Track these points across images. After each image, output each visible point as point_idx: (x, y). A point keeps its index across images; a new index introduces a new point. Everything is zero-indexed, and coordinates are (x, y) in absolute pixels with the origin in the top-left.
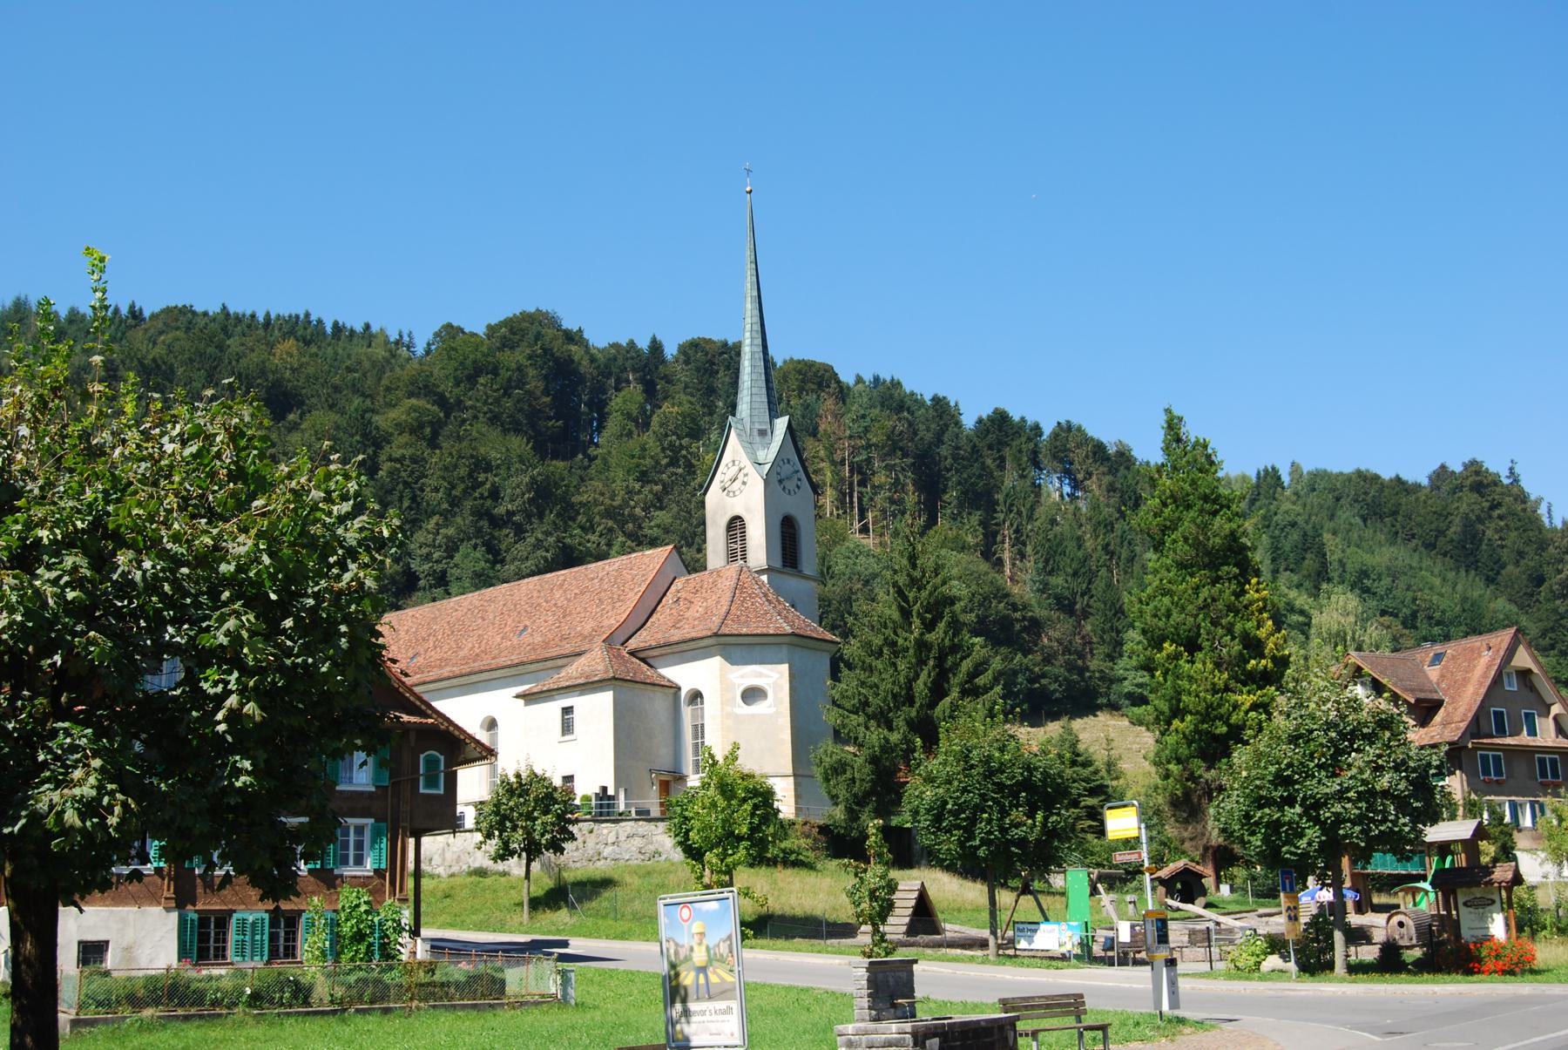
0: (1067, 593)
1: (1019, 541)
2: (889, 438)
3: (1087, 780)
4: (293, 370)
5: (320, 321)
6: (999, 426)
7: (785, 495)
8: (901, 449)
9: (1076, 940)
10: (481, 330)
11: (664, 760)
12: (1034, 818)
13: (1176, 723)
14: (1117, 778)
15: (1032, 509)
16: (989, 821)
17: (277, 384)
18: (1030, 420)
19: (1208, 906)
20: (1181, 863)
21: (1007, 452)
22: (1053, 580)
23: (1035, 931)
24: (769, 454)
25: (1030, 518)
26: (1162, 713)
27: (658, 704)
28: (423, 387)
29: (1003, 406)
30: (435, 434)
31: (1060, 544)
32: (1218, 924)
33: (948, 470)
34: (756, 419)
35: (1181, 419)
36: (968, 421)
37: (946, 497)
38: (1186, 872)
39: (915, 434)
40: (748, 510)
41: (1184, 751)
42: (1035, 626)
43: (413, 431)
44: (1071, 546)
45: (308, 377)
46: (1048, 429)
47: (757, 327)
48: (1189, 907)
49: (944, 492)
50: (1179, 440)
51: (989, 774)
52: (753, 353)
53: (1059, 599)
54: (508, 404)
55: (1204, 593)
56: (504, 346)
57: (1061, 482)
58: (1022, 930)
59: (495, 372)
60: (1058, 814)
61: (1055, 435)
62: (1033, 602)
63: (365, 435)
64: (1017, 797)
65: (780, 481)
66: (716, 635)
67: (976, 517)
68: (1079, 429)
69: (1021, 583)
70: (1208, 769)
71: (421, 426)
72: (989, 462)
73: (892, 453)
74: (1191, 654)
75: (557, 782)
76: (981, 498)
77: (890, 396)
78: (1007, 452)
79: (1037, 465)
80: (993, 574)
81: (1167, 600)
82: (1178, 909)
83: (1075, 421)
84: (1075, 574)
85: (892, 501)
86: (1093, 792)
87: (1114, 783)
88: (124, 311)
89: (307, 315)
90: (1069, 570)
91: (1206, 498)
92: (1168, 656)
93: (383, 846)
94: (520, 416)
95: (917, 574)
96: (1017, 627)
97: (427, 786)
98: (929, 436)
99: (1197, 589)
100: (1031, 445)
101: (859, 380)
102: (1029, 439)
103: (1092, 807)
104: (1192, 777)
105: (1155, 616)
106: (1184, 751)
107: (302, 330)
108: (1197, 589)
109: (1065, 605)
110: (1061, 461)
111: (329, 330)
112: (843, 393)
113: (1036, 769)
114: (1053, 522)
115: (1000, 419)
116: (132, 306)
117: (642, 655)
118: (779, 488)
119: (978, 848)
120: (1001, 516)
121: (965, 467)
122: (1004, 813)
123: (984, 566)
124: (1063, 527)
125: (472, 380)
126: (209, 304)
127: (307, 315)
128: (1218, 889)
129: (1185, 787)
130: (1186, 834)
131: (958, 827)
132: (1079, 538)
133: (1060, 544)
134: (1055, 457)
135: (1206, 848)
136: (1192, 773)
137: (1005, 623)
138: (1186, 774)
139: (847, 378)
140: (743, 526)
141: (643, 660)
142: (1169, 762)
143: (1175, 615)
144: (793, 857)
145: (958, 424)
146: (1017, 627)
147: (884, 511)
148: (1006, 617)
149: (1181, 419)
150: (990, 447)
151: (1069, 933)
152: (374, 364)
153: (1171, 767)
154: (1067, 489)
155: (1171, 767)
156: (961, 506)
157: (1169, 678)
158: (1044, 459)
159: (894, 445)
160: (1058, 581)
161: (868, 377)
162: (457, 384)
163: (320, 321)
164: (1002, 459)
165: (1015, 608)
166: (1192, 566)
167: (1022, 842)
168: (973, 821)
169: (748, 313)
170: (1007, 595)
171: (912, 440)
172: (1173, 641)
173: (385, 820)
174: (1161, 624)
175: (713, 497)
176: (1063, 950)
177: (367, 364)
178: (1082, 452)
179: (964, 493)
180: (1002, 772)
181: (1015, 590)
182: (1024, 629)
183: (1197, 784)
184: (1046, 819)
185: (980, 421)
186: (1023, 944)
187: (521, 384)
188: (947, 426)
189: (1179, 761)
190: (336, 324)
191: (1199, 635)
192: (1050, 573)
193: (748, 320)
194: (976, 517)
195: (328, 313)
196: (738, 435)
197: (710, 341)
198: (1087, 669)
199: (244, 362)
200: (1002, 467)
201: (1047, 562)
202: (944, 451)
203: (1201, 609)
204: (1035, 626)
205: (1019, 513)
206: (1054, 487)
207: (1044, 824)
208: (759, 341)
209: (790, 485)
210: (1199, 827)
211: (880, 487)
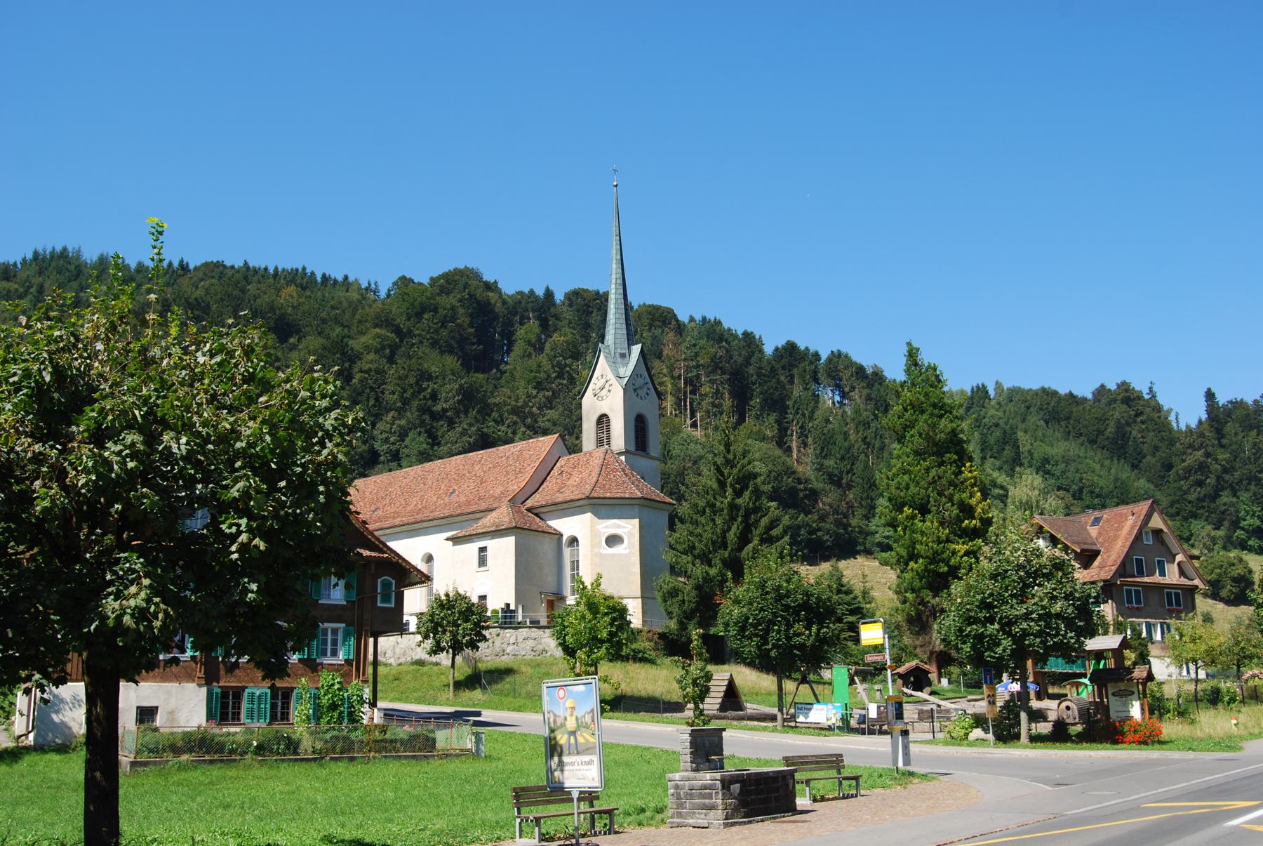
1: (803, 435)
3: (848, 604)
4: (294, 308)
5: (313, 273)
6: (790, 352)
7: (638, 400)
9: (839, 716)
11: (550, 586)
13: (912, 564)
15: (813, 412)
16: (779, 632)
18: (812, 349)
19: (932, 693)
20: (914, 663)
21: (795, 371)
22: (827, 462)
24: (627, 371)
25: (811, 418)
27: (547, 545)
28: (384, 320)
29: (792, 339)
33: (754, 384)
36: (769, 349)
37: (752, 403)
39: (731, 358)
40: (612, 410)
41: (917, 584)
42: (814, 495)
44: (839, 438)
45: (304, 312)
46: (824, 356)
47: (620, 281)
49: (751, 399)
50: (916, 365)
51: (779, 598)
53: (830, 475)
55: (933, 472)
59: (435, 310)
61: (830, 360)
66: (588, 498)
67: (772, 418)
68: (846, 356)
70: (934, 597)
71: (383, 348)
72: (782, 378)
73: (714, 372)
74: (923, 515)
76: (776, 404)
77: (713, 331)
78: (795, 371)
79: (817, 381)
80: (784, 458)
81: (906, 477)
83: (844, 350)
84: (842, 458)
88: (176, 264)
89: (304, 269)
91: (935, 406)
94: (452, 342)
95: (731, 457)
96: (801, 495)
98: (740, 360)
99: (927, 470)
100: (813, 367)
101: (692, 319)
102: (811, 363)
103: (852, 623)
104: (923, 603)
106: (917, 584)
108: (927, 470)
109: (834, 480)
111: (319, 279)
112: (680, 328)
114: (827, 421)
115: (791, 348)
116: (182, 261)
118: (634, 395)
122: (789, 626)
123: (778, 452)
124: (835, 424)
126: (234, 259)
127: (304, 269)
128: (939, 681)
129: (917, 609)
132: (845, 433)
134: (829, 375)
135: (932, 653)
136: (922, 600)
137: (793, 492)
139: (683, 317)
140: (608, 421)
141: (536, 515)
145: (761, 351)
146: (801, 495)
150: (784, 368)
152: (350, 303)
153: (907, 595)
154: (837, 398)
155: (907, 595)
156: (762, 409)
158: (822, 376)
159: (715, 366)
160: (830, 463)
164: (792, 377)
167: (802, 647)
168: (767, 631)
170: (794, 473)
172: (910, 506)
174: (902, 494)
175: (587, 400)
176: (830, 723)
179: (765, 400)
182: (806, 497)
184: (819, 630)
185: (777, 349)
188: (753, 353)
189: (913, 591)
190: (324, 276)
192: (825, 458)
194: (772, 418)
195: (318, 267)
197: (587, 290)
198: (850, 525)
199: (259, 301)
200: (791, 382)
201: (822, 449)
202: (751, 370)
204: (814, 495)
205: (804, 415)
206: (829, 397)
211: (706, 395)
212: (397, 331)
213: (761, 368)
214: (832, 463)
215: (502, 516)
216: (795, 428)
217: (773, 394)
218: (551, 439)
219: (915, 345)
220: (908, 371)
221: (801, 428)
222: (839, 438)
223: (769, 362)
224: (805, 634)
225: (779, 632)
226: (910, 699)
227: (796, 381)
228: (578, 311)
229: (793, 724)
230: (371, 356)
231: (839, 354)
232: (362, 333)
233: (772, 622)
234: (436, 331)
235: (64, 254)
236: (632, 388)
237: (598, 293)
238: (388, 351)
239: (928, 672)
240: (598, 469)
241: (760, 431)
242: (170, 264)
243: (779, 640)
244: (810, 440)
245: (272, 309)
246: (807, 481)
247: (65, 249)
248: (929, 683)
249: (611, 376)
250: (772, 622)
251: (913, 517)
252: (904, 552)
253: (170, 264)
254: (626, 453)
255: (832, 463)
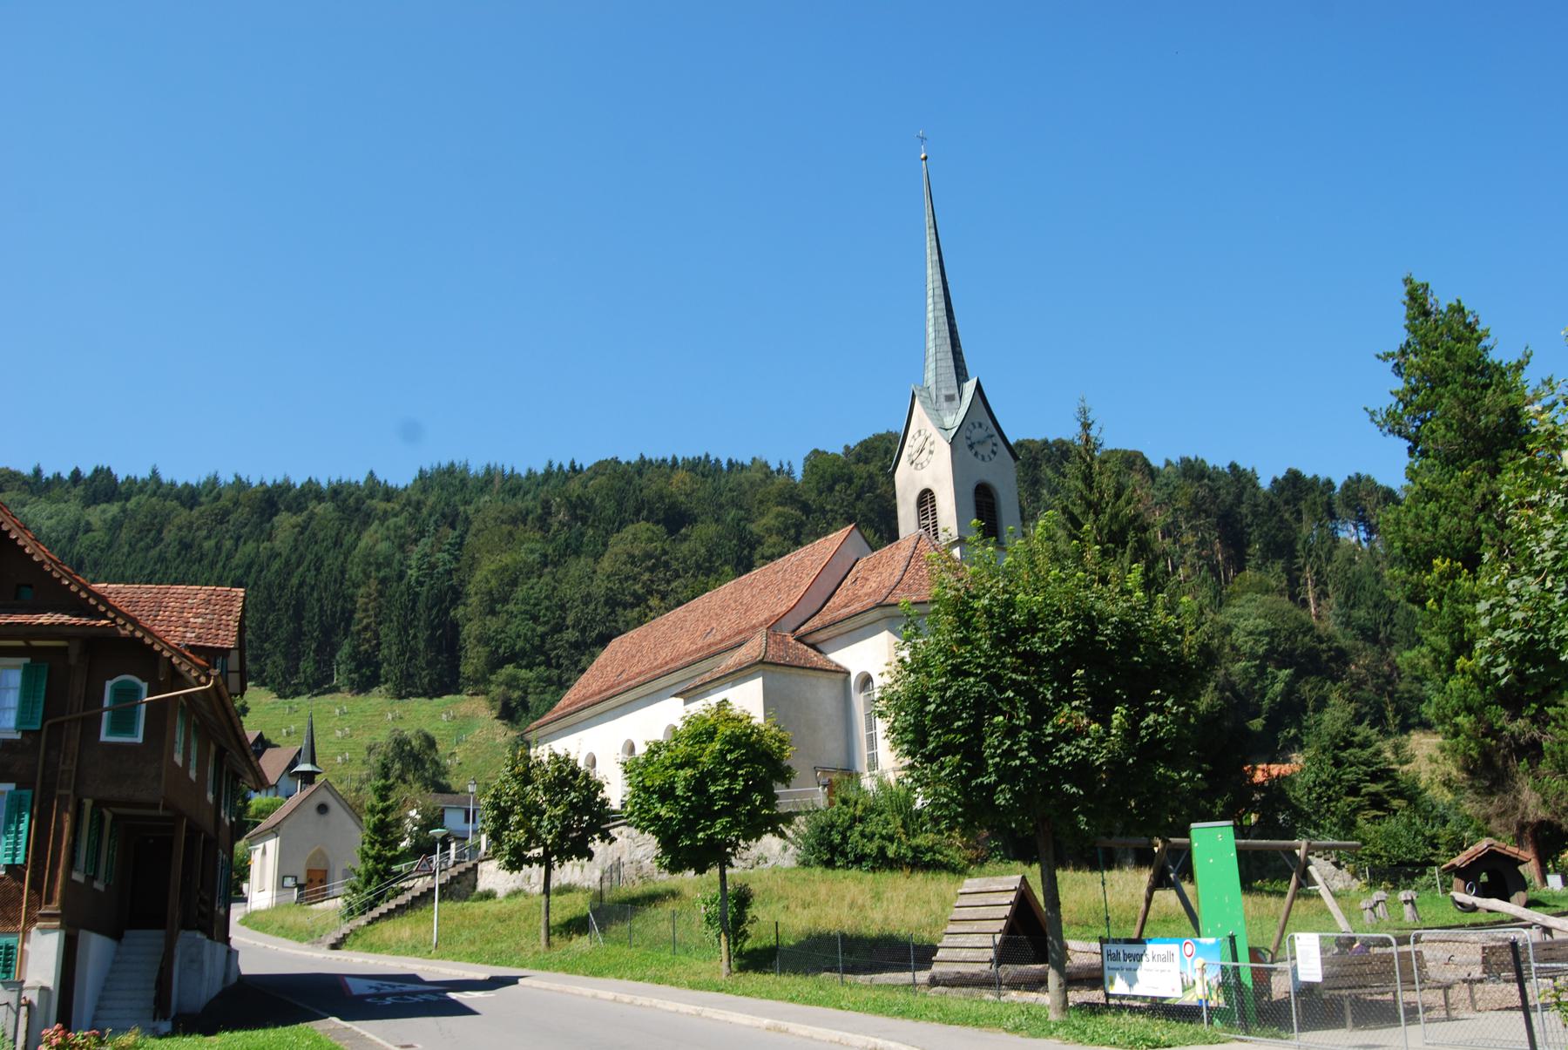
0: (1369, 624)
1: (1320, 581)
2: (1192, 502)
3: (1367, 763)
4: (687, 495)
5: (717, 460)
6: (1294, 483)
7: (978, 461)
8: (1205, 511)
9: (1214, 976)
10: (840, 451)
11: (835, 758)
12: (1106, 722)
13: (1461, 662)
14: (1407, 762)
15: (1330, 552)
16: (1011, 732)
17: (673, 506)
18: (1322, 476)
19: (1530, 904)
20: (1484, 844)
21: (1302, 505)
22: (1356, 613)
23: (1138, 958)
24: (954, 420)
25: (1329, 560)
26: (1441, 652)
27: (823, 692)
28: (790, 496)
29: (1295, 467)
30: (798, 534)
31: (1359, 580)
32: (1547, 930)
33: (1249, 526)
34: (942, 385)
35: (1426, 287)
36: (1265, 483)
37: (1250, 551)
38: (1491, 856)
39: (1217, 497)
40: (936, 480)
41: (1475, 696)
42: (1342, 656)
43: (779, 533)
44: (1369, 580)
45: (699, 500)
46: (1339, 483)
47: (940, 291)
48: (1494, 903)
49: (1248, 545)
50: (1427, 314)
51: (1008, 637)
52: (936, 318)
53: (1363, 630)
54: (860, 505)
55: (1481, 488)
56: (859, 461)
57: (1356, 527)
58: (1115, 957)
59: (850, 481)
60: (1160, 710)
61: (1346, 486)
62: (1339, 634)
63: (741, 539)
64: (1067, 680)
65: (971, 446)
66: (879, 606)
67: (1279, 566)
68: (1368, 479)
69: (1326, 617)
70: (1513, 718)
71: (787, 529)
72: (1287, 516)
73: (1197, 515)
74: (1472, 570)
75: (581, 764)
76: (1282, 549)
77: (1193, 470)
78: (1302, 505)
79: (1333, 516)
80: (1297, 611)
81: (1432, 506)
82: (1474, 909)
83: (1364, 473)
84: (1376, 606)
85: (1199, 557)
86: (1375, 777)
87: (1406, 768)
88: (567, 467)
89: (707, 456)
90: (1370, 603)
91: (1469, 370)
92: (1441, 575)
93: (24, 827)
94: (872, 515)
95: (1095, 497)
96: (1325, 657)
97: (115, 728)
98: (1230, 499)
99: (1470, 485)
100: (1325, 498)
101: (1168, 463)
102: (1322, 493)
103: (1376, 794)
104: (1491, 732)
105: (1417, 526)
106: (1475, 696)
107: (702, 468)
108: (1470, 485)
109: (1369, 635)
110: (1354, 508)
111: (725, 466)
112: (1151, 473)
113: (1103, 619)
114: (1351, 561)
115: (1294, 478)
116: (573, 462)
117: (810, 640)
118: (970, 454)
119: (991, 789)
120: (1302, 561)
121: (1265, 522)
122: (1040, 713)
123: (1286, 603)
124: (1361, 565)
125: (831, 489)
126: (628, 455)
127: (707, 456)
128: (1544, 881)
129: (1482, 746)
130: (1490, 810)
131: (948, 749)
132: (1377, 574)
133: (1359, 580)
134: (1348, 505)
135: (1522, 827)
136: (1491, 726)
137: (1312, 655)
138: (1482, 729)
139: (1157, 462)
140: (933, 499)
141: (813, 646)
142: (1457, 714)
143: (1443, 520)
144: (928, 858)
145: (1255, 486)
146: (1325, 657)
147: (1193, 566)
148: (1311, 649)
149: (1426, 287)
150: (1287, 502)
151: (1199, 962)
152: (752, 484)
153: (1459, 719)
154: (1363, 535)
155: (1459, 719)
156: (1265, 558)
157: (1446, 601)
158: (1339, 509)
159: (1198, 508)
160: (1360, 613)
161: (1175, 459)
162: (820, 493)
163: (717, 460)
164: (1299, 512)
165: (1320, 640)
166: (1461, 457)
167: (1081, 770)
168: (975, 731)
169: (930, 279)
170: (1312, 628)
171: (1214, 503)
172: (1445, 556)
173: (31, 785)
174: (1427, 536)
175: (903, 474)
176: (1191, 999)
177: (747, 486)
178: (1373, 499)
179: (1267, 545)
180: (1035, 631)
181: (1322, 626)
182: (1331, 659)
183: (1499, 740)
184: (1134, 721)
185: (1275, 481)
186: (1119, 987)
187: (872, 488)
188: (1244, 488)
189: (1469, 710)
190: (730, 461)
191: (1480, 542)
192: (1353, 607)
193: (930, 286)
194: (1279, 566)
195: (722, 453)
196: (923, 403)
197: (1033, 441)
198: (1396, 691)
199: (645, 492)
200: (1299, 520)
201: (1348, 597)
202: (1244, 509)
203: (1481, 510)
204: (1342, 656)
205: (1318, 557)
206: (1349, 534)
207: (1131, 732)
208: (943, 305)
209: (985, 450)
210: (1509, 798)
211: (1188, 546)
212: (806, 508)
213: (1256, 505)
214: (1362, 613)
215: (753, 649)
216: (1308, 574)
217: (1274, 537)
218: (836, 537)
219: (1418, 280)
220: (1412, 329)
221: (1317, 573)
222: (1369, 580)
223: (1266, 496)
224: (1089, 734)
225: (1011, 732)
226: (1470, 918)
227: (1305, 517)
228: (1023, 465)
229: (1096, 996)
230: (774, 539)
231: (1359, 478)
232: (762, 514)
233: (983, 707)
234: (852, 505)
235: (451, 470)
236: (965, 443)
237: (1046, 442)
238: (792, 532)
239: (1516, 862)
240: (904, 564)
241: (1261, 581)
242: (561, 467)
243: (1010, 754)
244: (1330, 588)
245: (661, 498)
246: (1330, 638)
247: (452, 464)
248: (1523, 885)
249: (931, 429)
250: (983, 707)
251: (1453, 574)
252: (1443, 642)
253: (561, 467)
254: (961, 542)
255: (1362, 613)
